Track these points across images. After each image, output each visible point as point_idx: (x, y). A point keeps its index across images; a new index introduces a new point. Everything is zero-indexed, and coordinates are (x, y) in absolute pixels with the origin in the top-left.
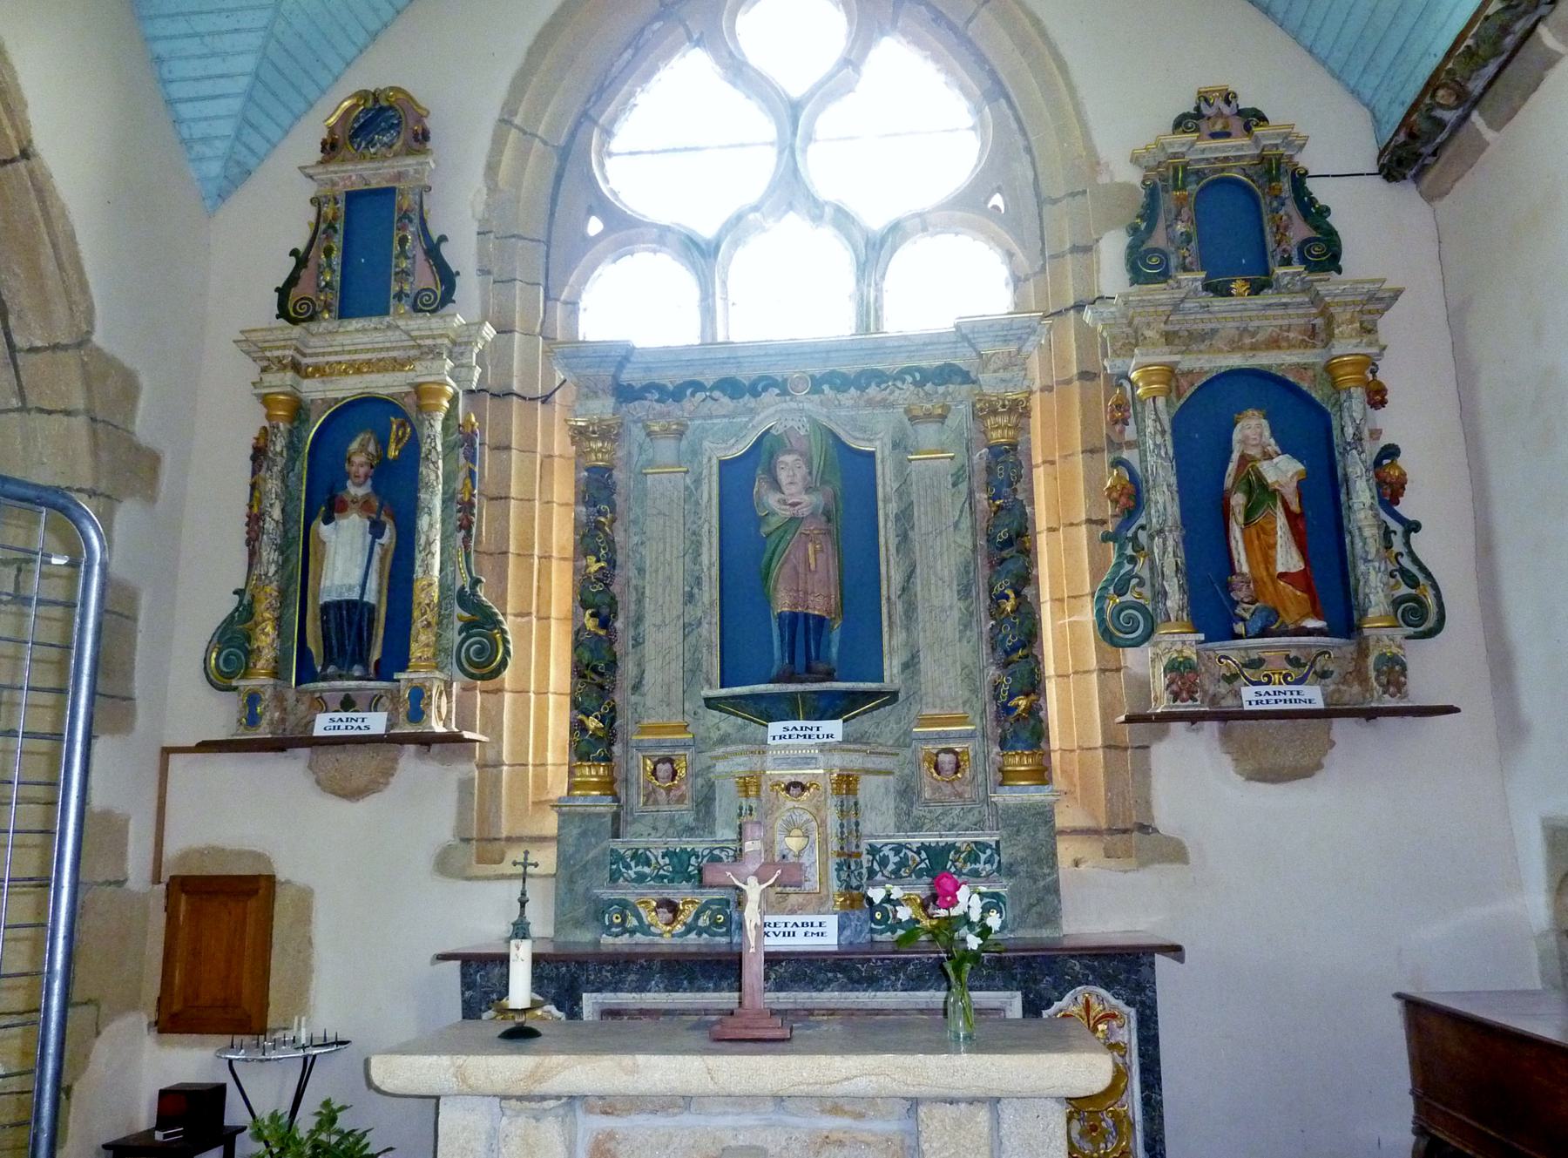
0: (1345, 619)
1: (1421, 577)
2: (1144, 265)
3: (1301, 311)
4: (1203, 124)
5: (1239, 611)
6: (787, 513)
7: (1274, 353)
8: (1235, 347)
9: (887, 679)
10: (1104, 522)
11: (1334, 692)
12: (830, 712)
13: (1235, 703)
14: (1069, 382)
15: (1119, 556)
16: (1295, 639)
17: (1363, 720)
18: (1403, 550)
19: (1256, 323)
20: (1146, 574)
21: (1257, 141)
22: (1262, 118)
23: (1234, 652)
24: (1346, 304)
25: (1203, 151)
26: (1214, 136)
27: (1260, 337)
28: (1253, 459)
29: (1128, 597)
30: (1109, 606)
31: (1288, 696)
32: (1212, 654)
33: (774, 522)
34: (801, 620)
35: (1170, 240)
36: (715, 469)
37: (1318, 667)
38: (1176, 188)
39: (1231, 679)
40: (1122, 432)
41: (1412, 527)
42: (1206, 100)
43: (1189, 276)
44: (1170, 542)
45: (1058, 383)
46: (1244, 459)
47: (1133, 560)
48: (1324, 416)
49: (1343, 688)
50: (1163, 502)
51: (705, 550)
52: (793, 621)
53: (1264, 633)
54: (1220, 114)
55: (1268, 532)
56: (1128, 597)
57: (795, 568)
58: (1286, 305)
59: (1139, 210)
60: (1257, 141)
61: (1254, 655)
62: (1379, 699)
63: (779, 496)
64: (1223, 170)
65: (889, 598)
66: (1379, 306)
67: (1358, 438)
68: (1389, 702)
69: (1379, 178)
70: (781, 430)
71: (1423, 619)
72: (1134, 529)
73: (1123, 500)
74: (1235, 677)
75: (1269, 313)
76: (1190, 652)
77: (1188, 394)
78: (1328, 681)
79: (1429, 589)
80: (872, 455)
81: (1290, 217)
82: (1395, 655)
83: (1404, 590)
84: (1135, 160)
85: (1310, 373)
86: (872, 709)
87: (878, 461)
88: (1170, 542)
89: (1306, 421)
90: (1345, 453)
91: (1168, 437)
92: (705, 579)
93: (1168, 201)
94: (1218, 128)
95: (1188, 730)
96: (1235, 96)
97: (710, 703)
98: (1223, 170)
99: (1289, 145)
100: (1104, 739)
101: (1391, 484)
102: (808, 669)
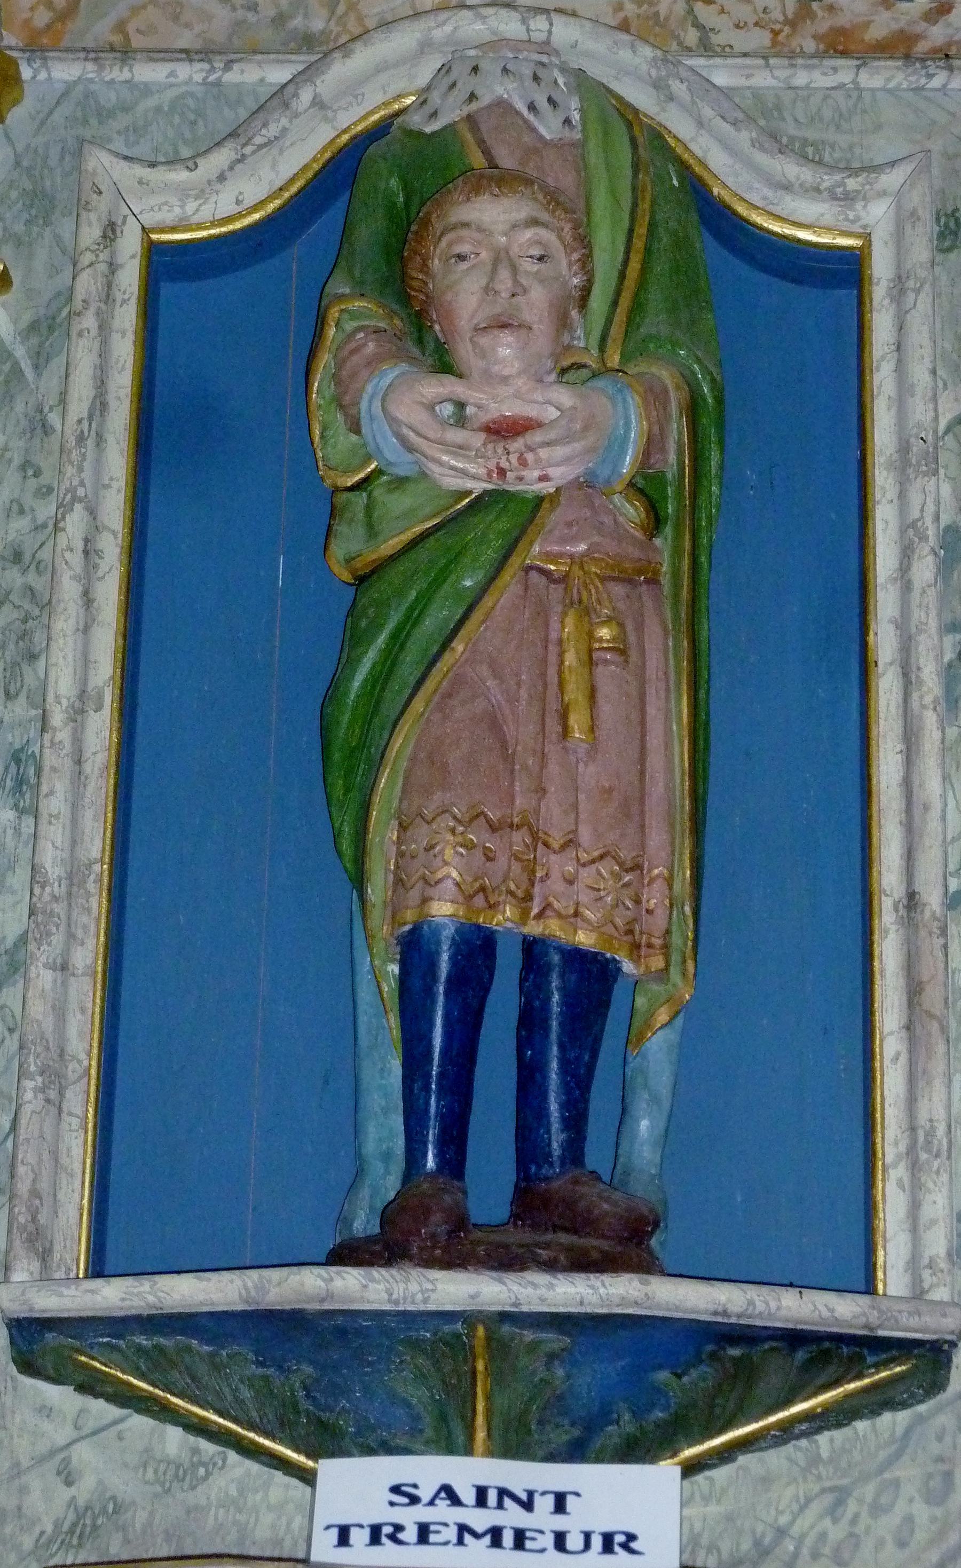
6: (462, 470)
9: (893, 1277)
10: (599, 890)
12: (612, 1434)
33: (403, 519)
34: (508, 965)
36: (130, 278)
51: (65, 623)
52: (453, 980)
57: (494, 723)
63: (435, 387)
65: (912, 900)
70: (452, 112)
80: (843, 272)
86: (819, 1421)
87: (879, 293)
92: (56, 760)
97: (41, 1345)
102: (530, 1202)
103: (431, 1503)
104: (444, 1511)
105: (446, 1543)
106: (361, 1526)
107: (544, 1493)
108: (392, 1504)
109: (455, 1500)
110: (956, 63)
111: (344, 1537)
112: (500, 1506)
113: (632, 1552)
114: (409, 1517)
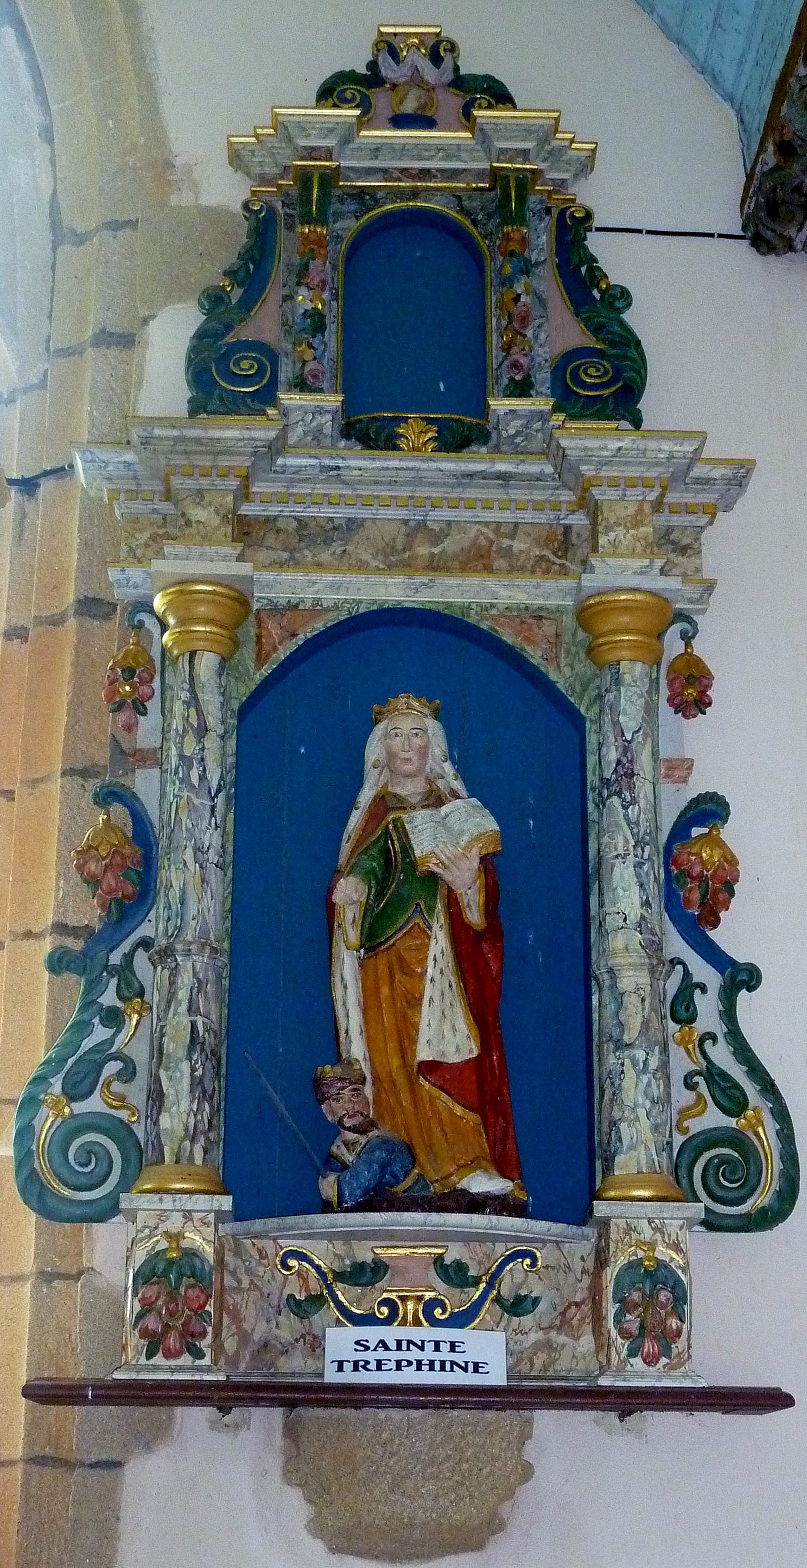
0: (562, 1173)
1: (751, 1090)
2: (224, 375)
3: (539, 496)
4: (381, 99)
5: (338, 1149)
7: (475, 580)
8: (395, 559)
11: (538, 1347)
13: (312, 1365)
14: (57, 621)
15: (87, 1005)
16: (435, 1218)
17: (612, 1417)
18: (718, 1027)
19: (447, 514)
20: (140, 1053)
21: (484, 137)
22: (501, 97)
23: (321, 1241)
24: (631, 483)
25: (376, 151)
26: (399, 121)
27: (451, 545)
28: (402, 804)
29: (95, 1104)
30: (46, 1123)
31: (429, 1354)
32: (268, 1245)
35: (287, 327)
37: (506, 1289)
38: (307, 219)
39: (304, 1307)
40: (130, 728)
41: (741, 978)
42: (393, 52)
43: (307, 400)
44: (186, 979)
45: (39, 621)
46: (385, 804)
47: (113, 1018)
48: (577, 722)
49: (562, 1339)
50: (194, 892)
53: (376, 1199)
54: (417, 80)
55: (409, 970)
56: (95, 1104)
58: (504, 477)
59: (231, 259)
60: (484, 137)
61: (364, 1253)
62: (620, 1370)
64: (415, 194)
66: (708, 498)
67: (627, 772)
68: (640, 1375)
69: (745, 244)
71: (750, 1187)
72: (126, 947)
73: (110, 880)
74: (317, 1301)
75: (470, 493)
76: (199, 1240)
77: (282, 654)
78: (527, 1321)
79: (767, 1117)
81: (542, 301)
82: (661, 1265)
83: (713, 1118)
84: (236, 158)
85: (548, 628)
88: (186, 979)
89: (527, 724)
90: (601, 803)
91: (212, 742)
93: (287, 245)
94: (410, 106)
95: (213, 1426)
96: (453, 48)
98: (415, 194)
99: (556, 155)
100: (30, 1442)
101: (701, 879)
103: (375, 1350)
104: (381, 1354)
105: (390, 1370)
106: (349, 1361)
107: (429, 1341)
108: (356, 1350)
109: (387, 1348)
110: (747, 1299)
111: (340, 1368)
112: (408, 1349)
113: (368, 1370)
114: (371, 1356)
